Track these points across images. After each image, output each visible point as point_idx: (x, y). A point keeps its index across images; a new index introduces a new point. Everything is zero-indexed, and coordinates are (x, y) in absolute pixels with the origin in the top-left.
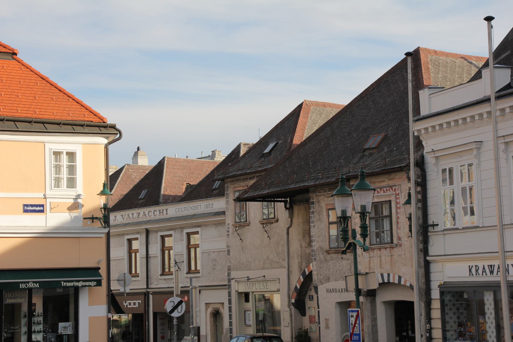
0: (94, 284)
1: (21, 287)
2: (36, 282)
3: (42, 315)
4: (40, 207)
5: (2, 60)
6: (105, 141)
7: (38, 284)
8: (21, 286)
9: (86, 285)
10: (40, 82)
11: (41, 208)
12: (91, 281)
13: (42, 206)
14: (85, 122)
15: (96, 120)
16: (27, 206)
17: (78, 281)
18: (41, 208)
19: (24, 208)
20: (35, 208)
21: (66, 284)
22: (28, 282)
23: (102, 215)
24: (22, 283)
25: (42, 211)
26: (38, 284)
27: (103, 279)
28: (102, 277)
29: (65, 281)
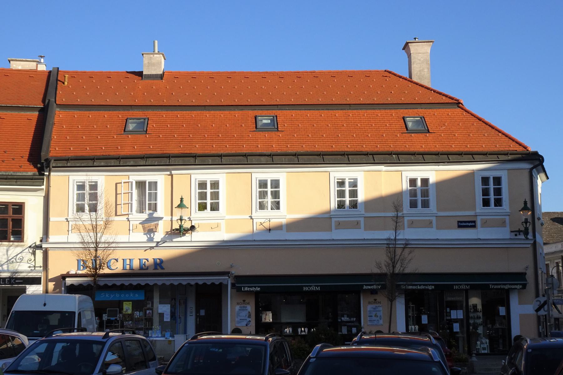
0: (519, 287)
1: (455, 288)
2: (318, 286)
3: (481, 310)
4: (472, 223)
5: (440, 109)
6: (531, 166)
7: (319, 287)
8: (455, 287)
9: (512, 287)
10: (476, 123)
11: (473, 224)
12: (517, 284)
13: (474, 222)
14: (509, 151)
15: (514, 147)
16: (461, 222)
17: (505, 284)
18: (473, 224)
19: (458, 224)
20: (468, 224)
21: (493, 287)
22: (461, 285)
23: (524, 228)
24: (305, 286)
25: (474, 226)
26: (319, 287)
27: (528, 283)
28: (527, 281)
29: (366, 285)
